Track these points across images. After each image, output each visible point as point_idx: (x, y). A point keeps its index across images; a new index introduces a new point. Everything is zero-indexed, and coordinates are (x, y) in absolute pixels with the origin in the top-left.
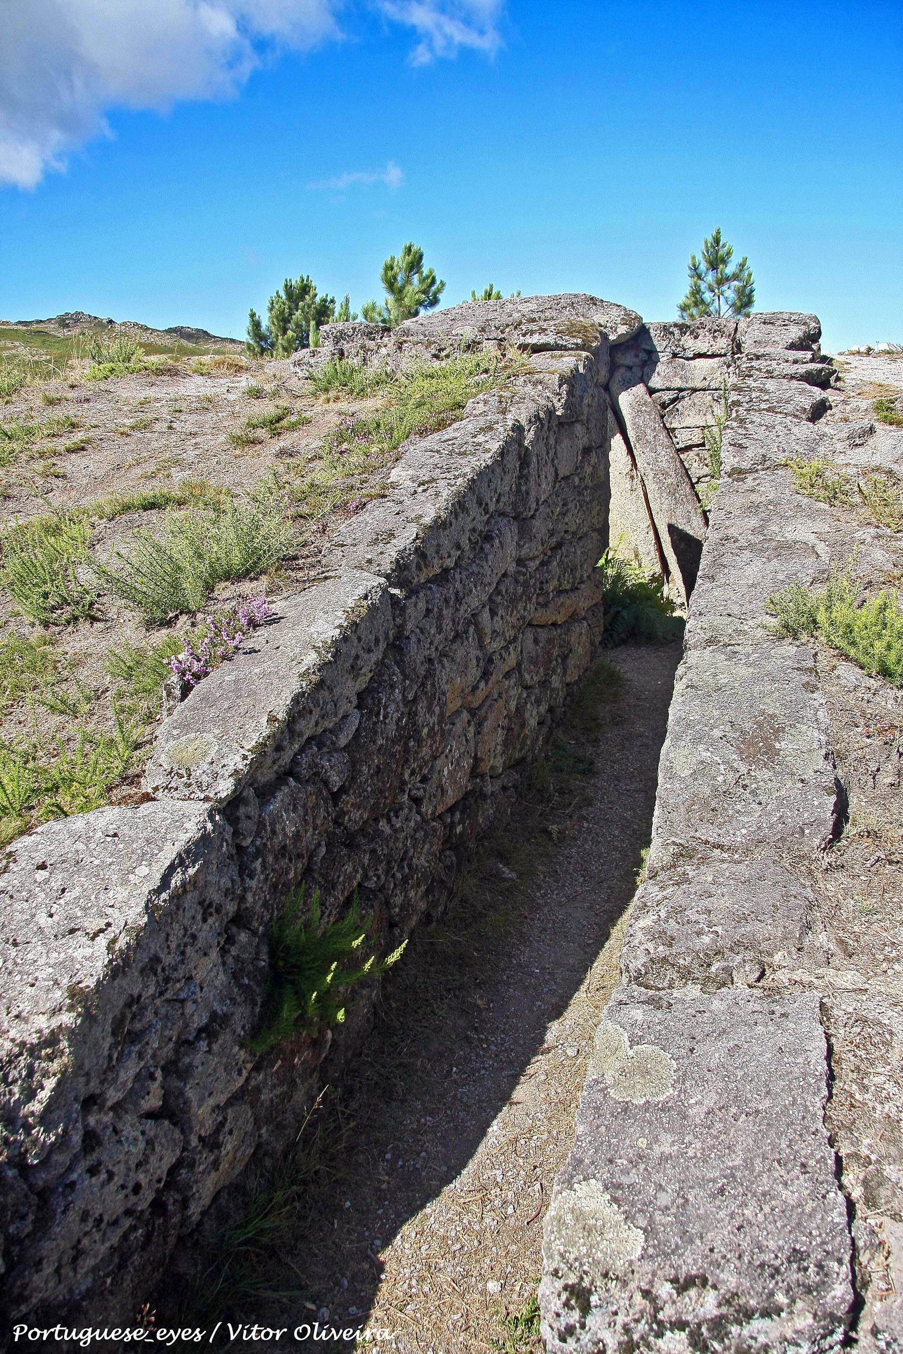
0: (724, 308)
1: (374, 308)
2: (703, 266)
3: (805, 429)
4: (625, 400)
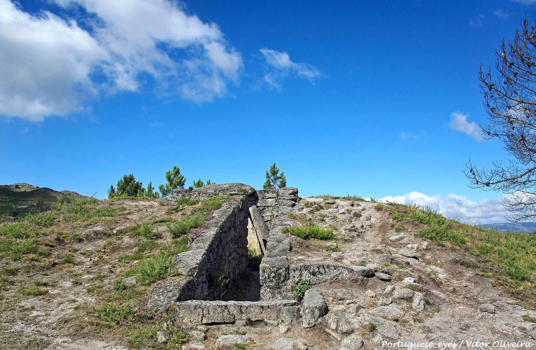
0: (277, 187)
1: (163, 186)
2: (270, 174)
3: (290, 208)
4: (251, 209)
